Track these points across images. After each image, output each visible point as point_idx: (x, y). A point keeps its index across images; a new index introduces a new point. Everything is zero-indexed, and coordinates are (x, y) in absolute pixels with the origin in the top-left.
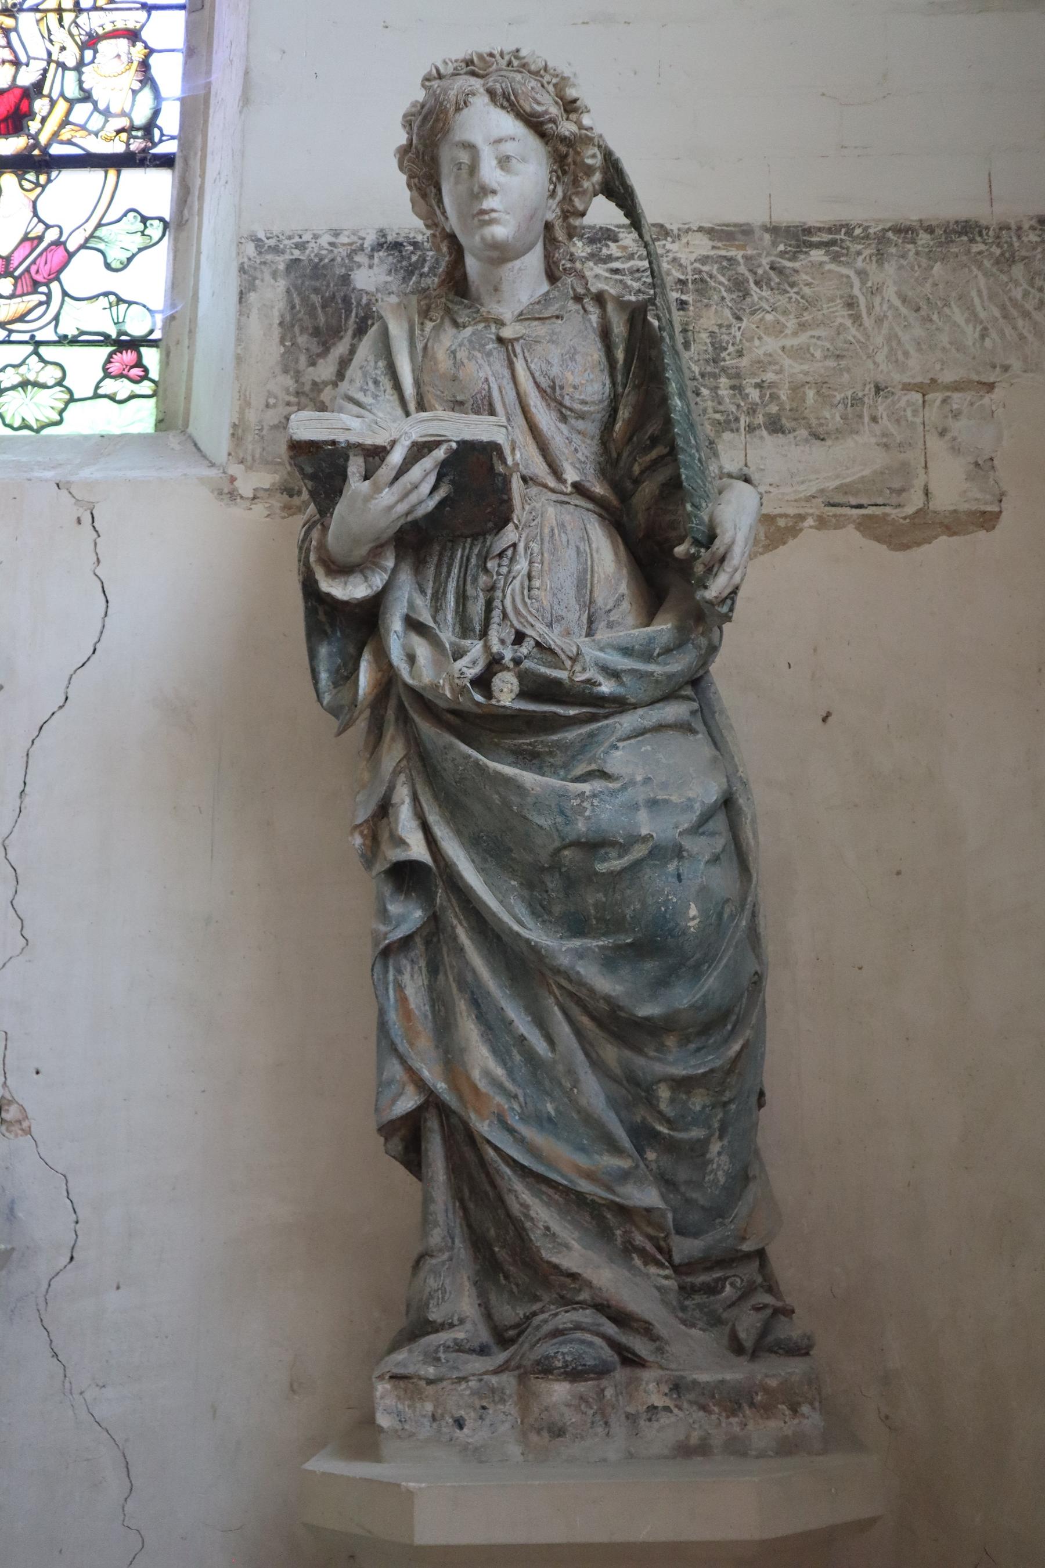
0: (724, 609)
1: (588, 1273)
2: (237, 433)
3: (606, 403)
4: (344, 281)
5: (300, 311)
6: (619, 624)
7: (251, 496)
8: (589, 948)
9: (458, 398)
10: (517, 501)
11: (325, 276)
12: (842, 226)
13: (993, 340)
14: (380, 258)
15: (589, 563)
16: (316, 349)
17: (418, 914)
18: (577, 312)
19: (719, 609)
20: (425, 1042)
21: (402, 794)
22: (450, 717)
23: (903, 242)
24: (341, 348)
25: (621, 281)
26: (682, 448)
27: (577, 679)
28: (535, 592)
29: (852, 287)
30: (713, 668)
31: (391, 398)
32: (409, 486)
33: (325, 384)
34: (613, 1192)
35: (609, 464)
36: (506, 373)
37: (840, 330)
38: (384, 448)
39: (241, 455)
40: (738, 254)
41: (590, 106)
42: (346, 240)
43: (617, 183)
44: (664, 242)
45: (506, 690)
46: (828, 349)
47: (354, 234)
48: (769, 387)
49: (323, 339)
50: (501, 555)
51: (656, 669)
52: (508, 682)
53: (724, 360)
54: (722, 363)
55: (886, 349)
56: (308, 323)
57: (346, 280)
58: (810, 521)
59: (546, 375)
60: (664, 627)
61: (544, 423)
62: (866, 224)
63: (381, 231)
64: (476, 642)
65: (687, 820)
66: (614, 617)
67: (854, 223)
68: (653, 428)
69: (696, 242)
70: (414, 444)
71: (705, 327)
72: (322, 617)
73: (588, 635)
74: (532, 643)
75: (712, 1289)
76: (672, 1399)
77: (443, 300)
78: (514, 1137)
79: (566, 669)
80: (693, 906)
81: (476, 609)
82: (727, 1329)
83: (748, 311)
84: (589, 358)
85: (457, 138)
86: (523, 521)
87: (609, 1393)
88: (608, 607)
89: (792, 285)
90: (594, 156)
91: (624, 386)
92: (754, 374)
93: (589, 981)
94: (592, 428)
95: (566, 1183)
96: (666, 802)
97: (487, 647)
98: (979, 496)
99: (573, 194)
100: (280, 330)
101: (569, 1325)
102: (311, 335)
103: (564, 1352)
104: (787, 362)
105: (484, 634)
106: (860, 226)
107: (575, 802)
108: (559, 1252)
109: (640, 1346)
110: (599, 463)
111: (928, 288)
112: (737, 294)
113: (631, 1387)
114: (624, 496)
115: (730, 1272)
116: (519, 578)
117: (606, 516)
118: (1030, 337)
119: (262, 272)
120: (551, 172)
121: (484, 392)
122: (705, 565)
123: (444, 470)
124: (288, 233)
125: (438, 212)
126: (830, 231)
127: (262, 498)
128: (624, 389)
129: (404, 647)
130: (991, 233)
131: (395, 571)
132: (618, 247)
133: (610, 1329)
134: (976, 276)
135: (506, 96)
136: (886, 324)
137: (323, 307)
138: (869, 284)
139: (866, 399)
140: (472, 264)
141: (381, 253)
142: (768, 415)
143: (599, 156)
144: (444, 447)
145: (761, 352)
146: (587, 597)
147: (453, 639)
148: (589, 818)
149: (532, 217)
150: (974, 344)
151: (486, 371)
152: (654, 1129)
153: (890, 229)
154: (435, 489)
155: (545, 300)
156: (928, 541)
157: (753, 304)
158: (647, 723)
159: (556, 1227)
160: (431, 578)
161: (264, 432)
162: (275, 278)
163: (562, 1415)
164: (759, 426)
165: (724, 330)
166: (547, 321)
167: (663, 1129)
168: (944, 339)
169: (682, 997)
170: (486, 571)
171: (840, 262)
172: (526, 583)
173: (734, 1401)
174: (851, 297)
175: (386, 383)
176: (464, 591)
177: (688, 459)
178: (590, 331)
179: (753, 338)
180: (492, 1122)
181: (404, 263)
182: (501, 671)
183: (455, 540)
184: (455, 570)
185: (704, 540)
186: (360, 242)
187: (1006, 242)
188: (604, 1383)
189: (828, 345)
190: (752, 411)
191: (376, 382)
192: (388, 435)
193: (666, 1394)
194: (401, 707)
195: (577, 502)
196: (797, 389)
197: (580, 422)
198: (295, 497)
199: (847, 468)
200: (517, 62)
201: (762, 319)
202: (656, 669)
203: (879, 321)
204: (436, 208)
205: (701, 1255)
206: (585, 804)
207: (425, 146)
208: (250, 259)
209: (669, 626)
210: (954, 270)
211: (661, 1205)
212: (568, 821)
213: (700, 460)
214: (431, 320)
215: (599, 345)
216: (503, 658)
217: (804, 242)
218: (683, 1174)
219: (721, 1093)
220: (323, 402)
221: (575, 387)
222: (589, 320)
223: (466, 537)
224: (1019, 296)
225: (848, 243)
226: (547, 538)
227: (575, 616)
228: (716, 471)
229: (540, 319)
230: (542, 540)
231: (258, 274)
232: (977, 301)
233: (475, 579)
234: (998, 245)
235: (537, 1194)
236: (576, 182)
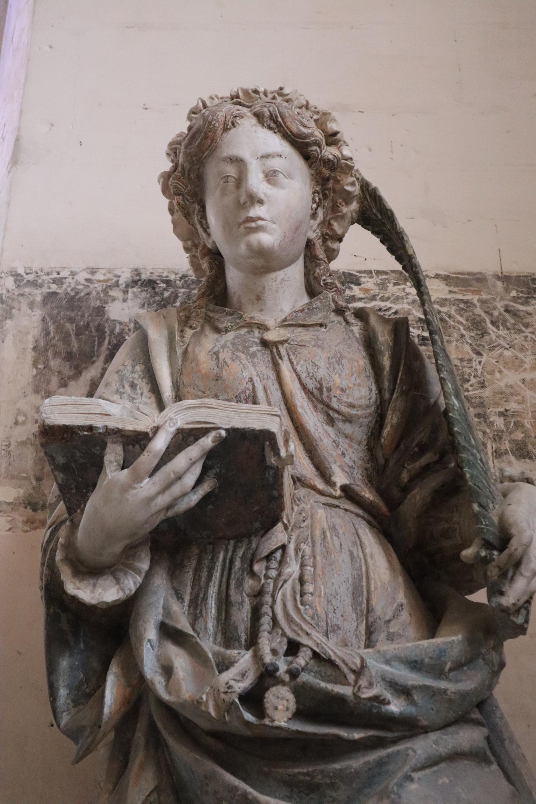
3: (373, 408)
4: (98, 312)
5: (54, 338)
6: (401, 636)
10: (287, 499)
11: (81, 307)
14: (134, 293)
15: (364, 569)
16: (67, 371)
19: (515, 619)
22: (210, 741)
24: (92, 372)
26: (464, 447)
27: (364, 696)
28: (308, 598)
30: (497, 692)
31: (149, 401)
32: (173, 476)
35: (377, 470)
36: (272, 375)
38: (146, 434)
40: (475, 299)
41: (348, 141)
42: (102, 278)
44: (403, 286)
45: (281, 706)
47: (109, 273)
48: (513, 415)
49: (75, 363)
50: (268, 558)
52: (282, 699)
53: (468, 391)
56: (61, 347)
57: (100, 311)
59: (312, 377)
60: (454, 638)
61: (311, 424)
63: (136, 270)
64: (243, 652)
66: (394, 628)
68: (421, 435)
70: (180, 432)
72: (65, 625)
73: (367, 646)
74: (309, 653)
77: (204, 310)
79: (348, 684)
81: (242, 616)
83: (487, 348)
84: (356, 363)
85: (225, 154)
86: (292, 521)
88: (388, 618)
89: (527, 326)
90: (353, 184)
92: (497, 404)
94: (359, 432)
97: (258, 658)
99: (332, 218)
100: (33, 354)
102: (64, 359)
105: (252, 642)
110: (366, 469)
112: (475, 332)
114: (393, 505)
116: (289, 583)
117: (375, 523)
119: (19, 302)
121: (248, 392)
122: (500, 568)
123: (211, 458)
124: (46, 270)
125: (200, 230)
127: (5, 512)
128: (392, 395)
129: (158, 658)
131: (148, 576)
132: (361, 289)
137: (77, 335)
140: (234, 277)
141: (135, 289)
142: (513, 442)
143: (358, 186)
144: (212, 435)
145: (502, 384)
146: (364, 605)
147: (217, 648)
149: (297, 228)
151: (250, 372)
154: (199, 482)
155: (308, 310)
157: (492, 341)
158: (442, 750)
160: (189, 583)
161: (12, 448)
164: (506, 452)
165: (465, 364)
170: (253, 574)
172: (298, 587)
175: (144, 386)
176: (228, 596)
178: (354, 340)
181: (157, 298)
182: (274, 685)
183: (216, 541)
184: (217, 575)
185: (496, 542)
186: (116, 279)
190: (498, 437)
191: (133, 386)
192: (151, 421)
194: (153, 728)
195: (347, 506)
197: (348, 425)
198: (39, 512)
201: (501, 355)
204: (198, 227)
207: (192, 163)
208: (8, 291)
209: (460, 637)
213: (481, 460)
214: (191, 327)
215: (364, 354)
216: (277, 669)
221: (343, 390)
223: (228, 540)
227: (351, 625)
228: (497, 474)
229: (303, 326)
230: (313, 542)
231: (16, 304)
233: (240, 584)
236: (335, 208)
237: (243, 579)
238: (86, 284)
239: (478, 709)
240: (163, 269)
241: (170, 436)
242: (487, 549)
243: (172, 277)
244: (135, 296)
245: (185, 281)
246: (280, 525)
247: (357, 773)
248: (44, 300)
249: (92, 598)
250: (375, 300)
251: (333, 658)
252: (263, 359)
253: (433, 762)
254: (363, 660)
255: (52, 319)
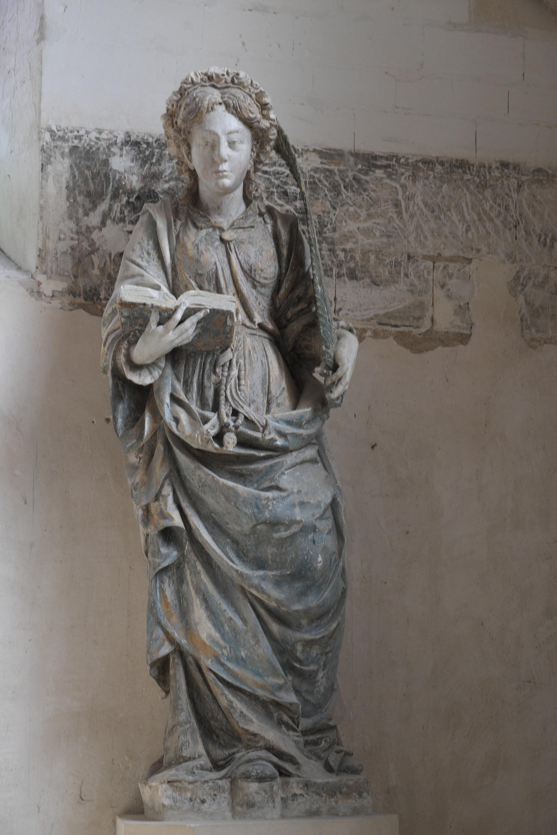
0: (339, 402)
1: (263, 733)
2: (42, 255)
4: (105, 163)
5: (78, 180)
7: (51, 295)
8: (267, 576)
9: (199, 272)
12: (394, 156)
13: (473, 233)
14: (127, 151)
16: (88, 205)
17: (175, 553)
18: (261, 222)
20: (175, 619)
21: (167, 490)
23: (427, 170)
25: (268, 179)
26: (321, 315)
28: (242, 388)
29: (398, 194)
33: (94, 228)
34: (274, 695)
35: (276, 313)
36: (226, 260)
37: (390, 220)
39: (44, 268)
40: (334, 168)
43: (284, 148)
45: (230, 442)
46: (383, 231)
47: (111, 133)
48: (350, 252)
50: (223, 366)
51: (302, 432)
53: (325, 233)
54: (324, 235)
55: (414, 235)
56: (83, 187)
57: (106, 163)
58: (369, 333)
62: (407, 156)
63: (127, 133)
65: (318, 512)
67: (400, 155)
68: (299, 291)
69: (312, 159)
70: (188, 309)
71: (315, 212)
74: (243, 417)
75: (316, 743)
76: (304, 790)
78: (224, 668)
79: (259, 431)
80: (320, 556)
82: (323, 762)
87: (275, 788)
88: (277, 395)
89: (365, 190)
91: (287, 270)
92: (342, 243)
93: (267, 592)
94: (268, 291)
95: (250, 690)
96: (308, 503)
98: (459, 324)
100: (66, 191)
101: (255, 757)
102: (86, 196)
103: (255, 769)
104: (360, 237)
105: (216, 408)
106: (404, 157)
107: (264, 502)
108: (248, 724)
109: (288, 767)
111: (439, 199)
113: (285, 785)
115: (325, 735)
118: (492, 233)
119: (55, 152)
120: (252, 146)
121: (213, 270)
124: (70, 128)
126: (387, 158)
130: (475, 169)
133: (275, 759)
134: (465, 194)
135: (235, 108)
136: (415, 219)
137: (93, 179)
138: (407, 193)
139: (403, 263)
141: (127, 148)
142: (349, 269)
144: (203, 312)
145: (346, 230)
148: (271, 511)
150: (462, 235)
151: (215, 259)
152: (293, 665)
153: (420, 161)
155: (245, 216)
156: (432, 348)
157: (343, 200)
159: (245, 711)
161: (58, 256)
162: (63, 158)
163: (254, 797)
165: (326, 215)
166: (247, 230)
167: (298, 666)
168: (446, 230)
169: (312, 601)
171: (392, 178)
173: (332, 791)
174: (397, 200)
175: (153, 253)
176: (203, 382)
177: (324, 321)
178: (268, 234)
179: (342, 221)
180: (212, 660)
181: (141, 155)
184: (197, 370)
187: (483, 175)
188: (273, 783)
189: (383, 229)
190: (340, 265)
191: (148, 253)
193: (301, 788)
196: (365, 254)
198: (77, 297)
199: (391, 303)
200: (235, 81)
201: (347, 210)
202: (302, 432)
203: (412, 216)
205: (311, 727)
206: (269, 503)
208: (47, 143)
209: (310, 409)
210: (454, 189)
211: (298, 702)
212: (261, 512)
214: (180, 220)
215: (273, 244)
216: (229, 425)
217: (372, 164)
218: (304, 687)
219: (326, 648)
220: (93, 240)
221: (262, 270)
222: (267, 228)
224: (488, 209)
225: (397, 167)
226: (247, 356)
227: (261, 400)
231: (53, 154)
232: (465, 209)
233: (209, 378)
234: (478, 177)
235: (236, 696)
237: (211, 375)
238: (96, 141)
239: (316, 440)
240: (145, 134)
241: (183, 312)
242: (327, 369)
243: (150, 140)
244: (128, 153)
245: (159, 144)
246: (229, 350)
247: (261, 470)
248: (70, 152)
249: (140, 381)
250: (275, 165)
251: (254, 419)
252: (222, 249)
253: (293, 466)
254: (267, 421)
255: (76, 166)
